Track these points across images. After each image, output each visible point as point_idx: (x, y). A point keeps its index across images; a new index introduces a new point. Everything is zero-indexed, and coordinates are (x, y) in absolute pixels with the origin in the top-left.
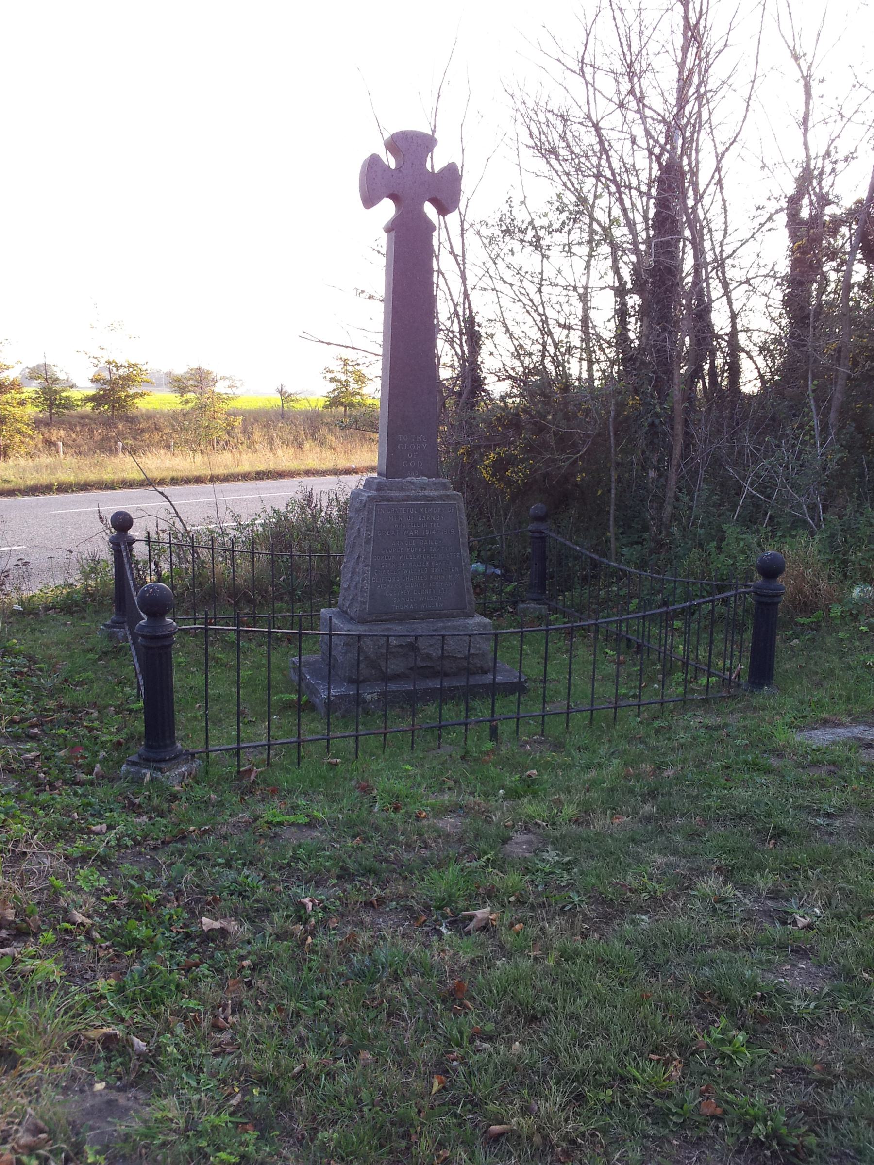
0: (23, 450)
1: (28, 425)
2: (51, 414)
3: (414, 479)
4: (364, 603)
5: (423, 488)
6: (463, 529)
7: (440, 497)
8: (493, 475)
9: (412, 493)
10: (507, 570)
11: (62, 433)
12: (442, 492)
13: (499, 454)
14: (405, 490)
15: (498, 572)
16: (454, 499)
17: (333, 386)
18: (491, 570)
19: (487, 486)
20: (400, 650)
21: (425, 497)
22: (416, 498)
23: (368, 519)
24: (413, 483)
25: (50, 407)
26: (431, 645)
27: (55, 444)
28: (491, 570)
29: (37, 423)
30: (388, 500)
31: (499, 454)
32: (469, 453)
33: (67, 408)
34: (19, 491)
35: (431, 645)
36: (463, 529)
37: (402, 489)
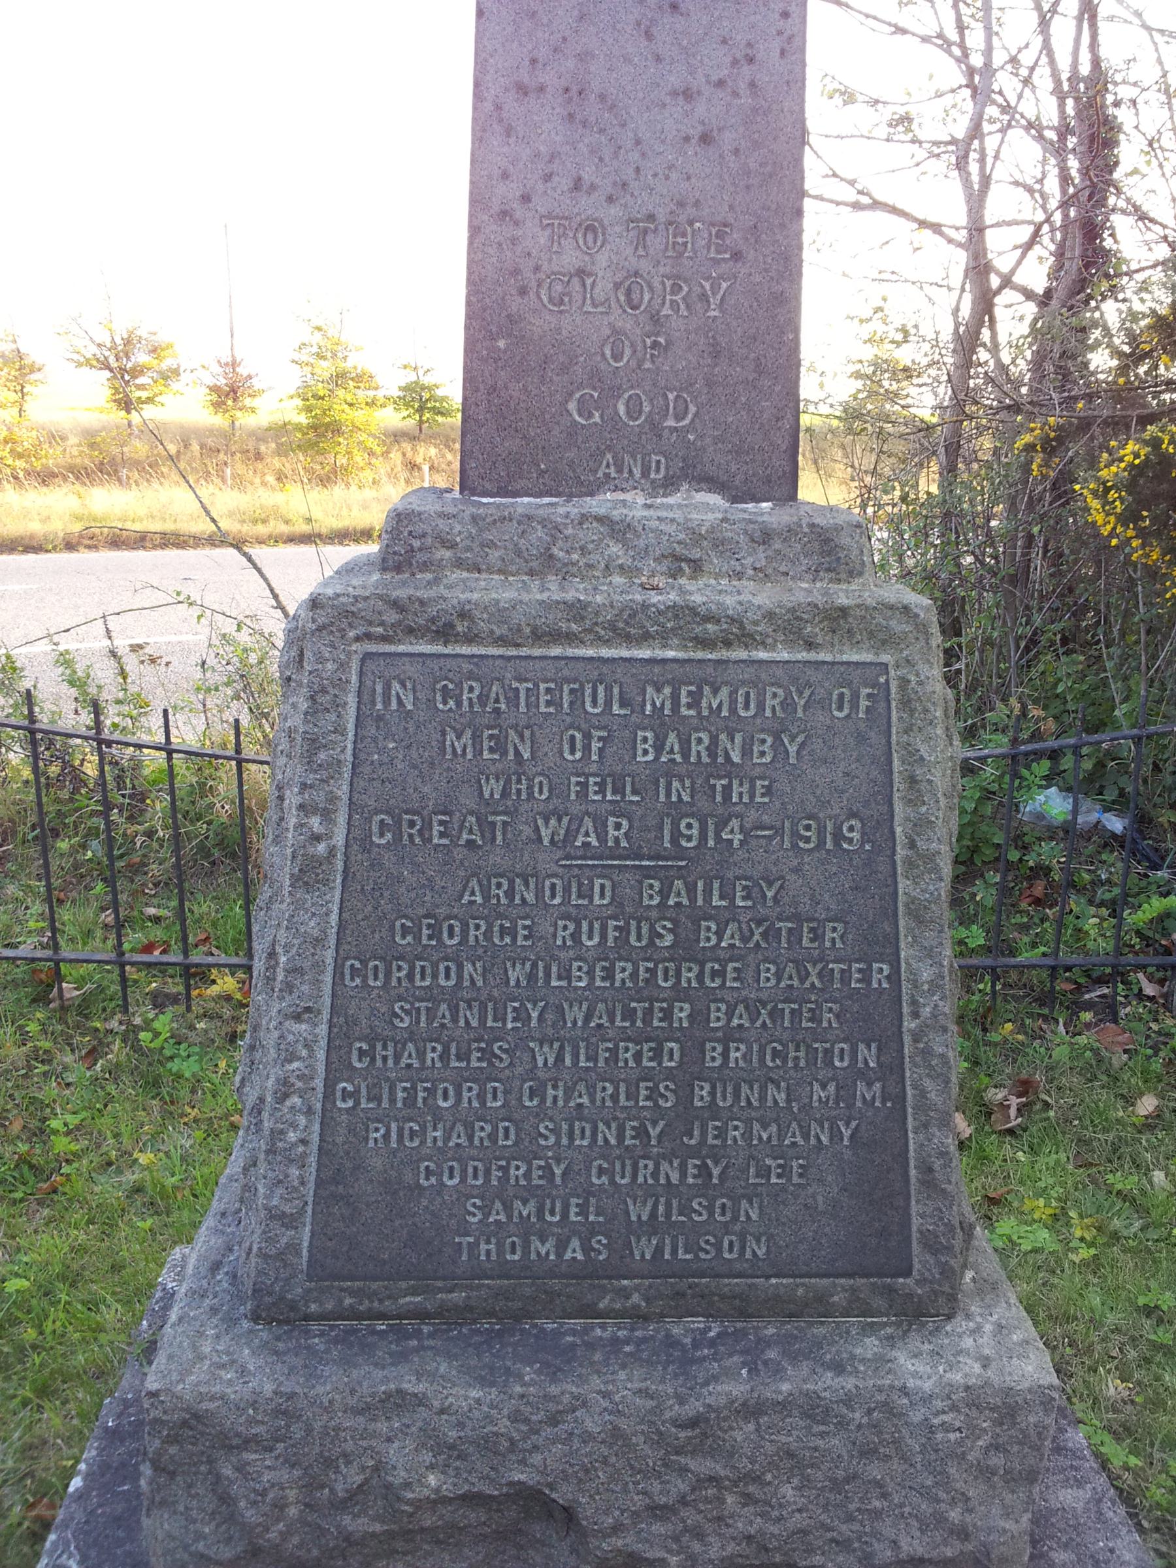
0: (368, 475)
1: (375, 437)
2: (421, 422)
3: (632, 504)
4: (290, 1221)
5: (682, 563)
6: (922, 824)
7: (790, 625)
8: (1129, 517)
9: (610, 593)
10: (1143, 822)
11: (433, 451)
12: (804, 591)
13: (1155, 443)
14: (566, 573)
15: (1116, 824)
16: (886, 640)
17: (859, 384)
18: (1090, 815)
19: (1102, 551)
20: (474, 1516)
21: (685, 621)
22: (628, 625)
23: (313, 744)
24: (618, 529)
25: (421, 410)
26: (657, 1511)
27: (420, 469)
28: (1090, 815)
29: (397, 437)
30: (445, 633)
31: (1155, 443)
32: (1051, 446)
33: (442, 414)
34: (320, 536)
35: (657, 1511)
36: (922, 824)
37: (545, 564)
